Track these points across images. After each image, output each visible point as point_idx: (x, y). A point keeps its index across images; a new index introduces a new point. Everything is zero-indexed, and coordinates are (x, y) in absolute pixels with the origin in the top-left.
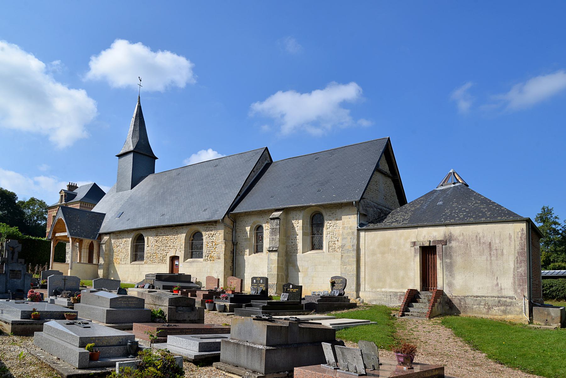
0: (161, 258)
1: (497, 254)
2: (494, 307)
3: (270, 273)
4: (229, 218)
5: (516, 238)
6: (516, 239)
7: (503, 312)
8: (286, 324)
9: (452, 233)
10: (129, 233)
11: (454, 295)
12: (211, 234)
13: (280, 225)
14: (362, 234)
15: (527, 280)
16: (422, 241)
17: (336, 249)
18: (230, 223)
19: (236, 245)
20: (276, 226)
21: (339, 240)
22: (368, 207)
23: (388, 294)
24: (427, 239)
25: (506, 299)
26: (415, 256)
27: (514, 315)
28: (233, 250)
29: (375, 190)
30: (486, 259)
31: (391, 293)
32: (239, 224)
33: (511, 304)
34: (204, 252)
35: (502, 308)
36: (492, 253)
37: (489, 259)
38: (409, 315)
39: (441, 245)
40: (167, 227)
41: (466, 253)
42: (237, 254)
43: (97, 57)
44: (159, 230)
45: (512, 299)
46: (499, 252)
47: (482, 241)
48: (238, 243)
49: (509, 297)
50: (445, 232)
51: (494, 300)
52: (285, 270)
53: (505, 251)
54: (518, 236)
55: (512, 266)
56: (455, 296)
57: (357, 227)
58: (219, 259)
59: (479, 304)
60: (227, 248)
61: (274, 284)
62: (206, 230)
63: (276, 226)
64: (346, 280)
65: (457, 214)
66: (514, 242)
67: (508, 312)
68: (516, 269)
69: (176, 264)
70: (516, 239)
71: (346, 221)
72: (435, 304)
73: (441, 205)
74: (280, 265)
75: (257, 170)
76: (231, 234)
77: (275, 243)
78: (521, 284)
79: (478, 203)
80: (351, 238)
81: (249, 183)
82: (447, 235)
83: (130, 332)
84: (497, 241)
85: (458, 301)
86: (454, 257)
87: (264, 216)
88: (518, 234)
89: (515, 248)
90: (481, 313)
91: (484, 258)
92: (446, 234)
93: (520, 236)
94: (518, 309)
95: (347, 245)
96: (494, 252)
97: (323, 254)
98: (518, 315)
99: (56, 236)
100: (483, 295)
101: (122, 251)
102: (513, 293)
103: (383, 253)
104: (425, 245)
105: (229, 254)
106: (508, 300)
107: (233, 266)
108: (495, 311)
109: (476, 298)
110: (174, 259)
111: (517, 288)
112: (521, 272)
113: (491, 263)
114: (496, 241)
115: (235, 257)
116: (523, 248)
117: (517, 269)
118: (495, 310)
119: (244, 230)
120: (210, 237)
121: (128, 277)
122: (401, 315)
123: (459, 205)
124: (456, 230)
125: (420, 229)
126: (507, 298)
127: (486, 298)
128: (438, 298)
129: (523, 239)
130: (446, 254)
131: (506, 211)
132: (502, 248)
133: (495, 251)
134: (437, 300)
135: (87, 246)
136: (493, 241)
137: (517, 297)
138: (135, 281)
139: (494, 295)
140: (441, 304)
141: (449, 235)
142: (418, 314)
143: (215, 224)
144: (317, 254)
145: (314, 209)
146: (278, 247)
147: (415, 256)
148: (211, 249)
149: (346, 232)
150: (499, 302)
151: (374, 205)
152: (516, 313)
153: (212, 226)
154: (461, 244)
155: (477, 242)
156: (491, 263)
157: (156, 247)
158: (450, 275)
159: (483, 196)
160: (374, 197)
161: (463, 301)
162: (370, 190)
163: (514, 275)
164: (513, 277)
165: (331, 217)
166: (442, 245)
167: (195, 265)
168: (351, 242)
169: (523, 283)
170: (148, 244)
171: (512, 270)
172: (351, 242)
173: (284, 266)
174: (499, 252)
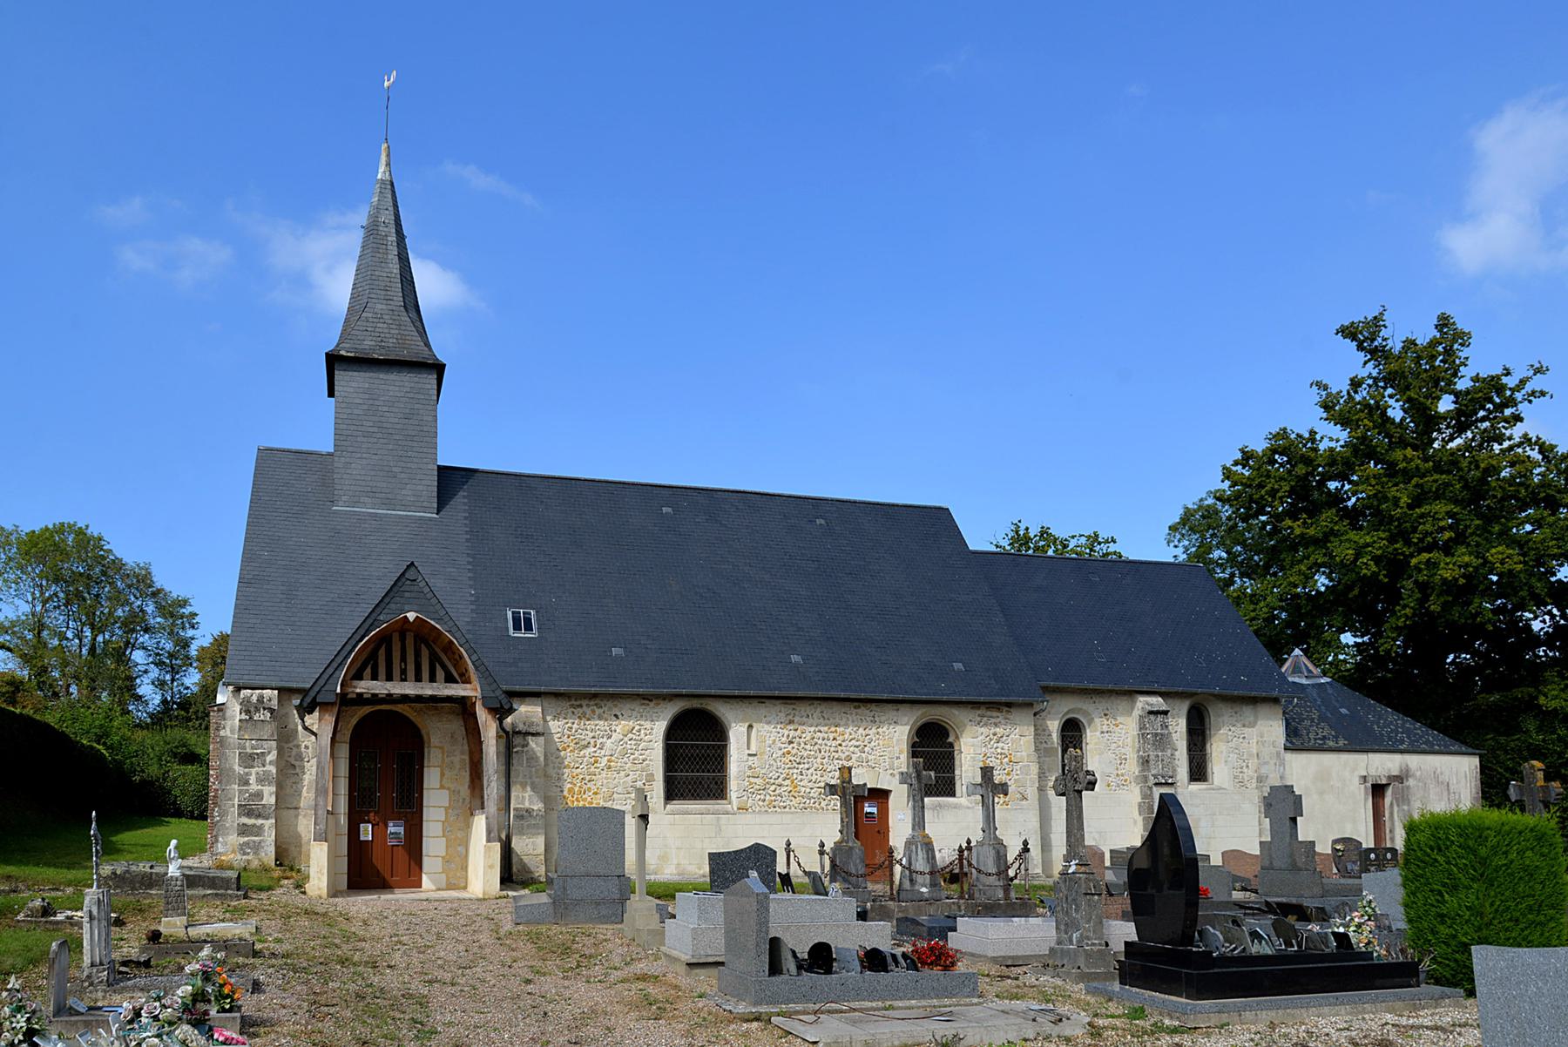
12: (995, 734)
21: (1250, 765)
44: (804, 709)
47: (1440, 780)
69: (867, 813)
80: (1276, 764)
87: (1097, 701)
89: (1471, 792)
103: (1321, 793)
119: (1041, 728)
124: (1414, 761)
143: (1007, 709)
147: (1366, 800)
153: (999, 714)
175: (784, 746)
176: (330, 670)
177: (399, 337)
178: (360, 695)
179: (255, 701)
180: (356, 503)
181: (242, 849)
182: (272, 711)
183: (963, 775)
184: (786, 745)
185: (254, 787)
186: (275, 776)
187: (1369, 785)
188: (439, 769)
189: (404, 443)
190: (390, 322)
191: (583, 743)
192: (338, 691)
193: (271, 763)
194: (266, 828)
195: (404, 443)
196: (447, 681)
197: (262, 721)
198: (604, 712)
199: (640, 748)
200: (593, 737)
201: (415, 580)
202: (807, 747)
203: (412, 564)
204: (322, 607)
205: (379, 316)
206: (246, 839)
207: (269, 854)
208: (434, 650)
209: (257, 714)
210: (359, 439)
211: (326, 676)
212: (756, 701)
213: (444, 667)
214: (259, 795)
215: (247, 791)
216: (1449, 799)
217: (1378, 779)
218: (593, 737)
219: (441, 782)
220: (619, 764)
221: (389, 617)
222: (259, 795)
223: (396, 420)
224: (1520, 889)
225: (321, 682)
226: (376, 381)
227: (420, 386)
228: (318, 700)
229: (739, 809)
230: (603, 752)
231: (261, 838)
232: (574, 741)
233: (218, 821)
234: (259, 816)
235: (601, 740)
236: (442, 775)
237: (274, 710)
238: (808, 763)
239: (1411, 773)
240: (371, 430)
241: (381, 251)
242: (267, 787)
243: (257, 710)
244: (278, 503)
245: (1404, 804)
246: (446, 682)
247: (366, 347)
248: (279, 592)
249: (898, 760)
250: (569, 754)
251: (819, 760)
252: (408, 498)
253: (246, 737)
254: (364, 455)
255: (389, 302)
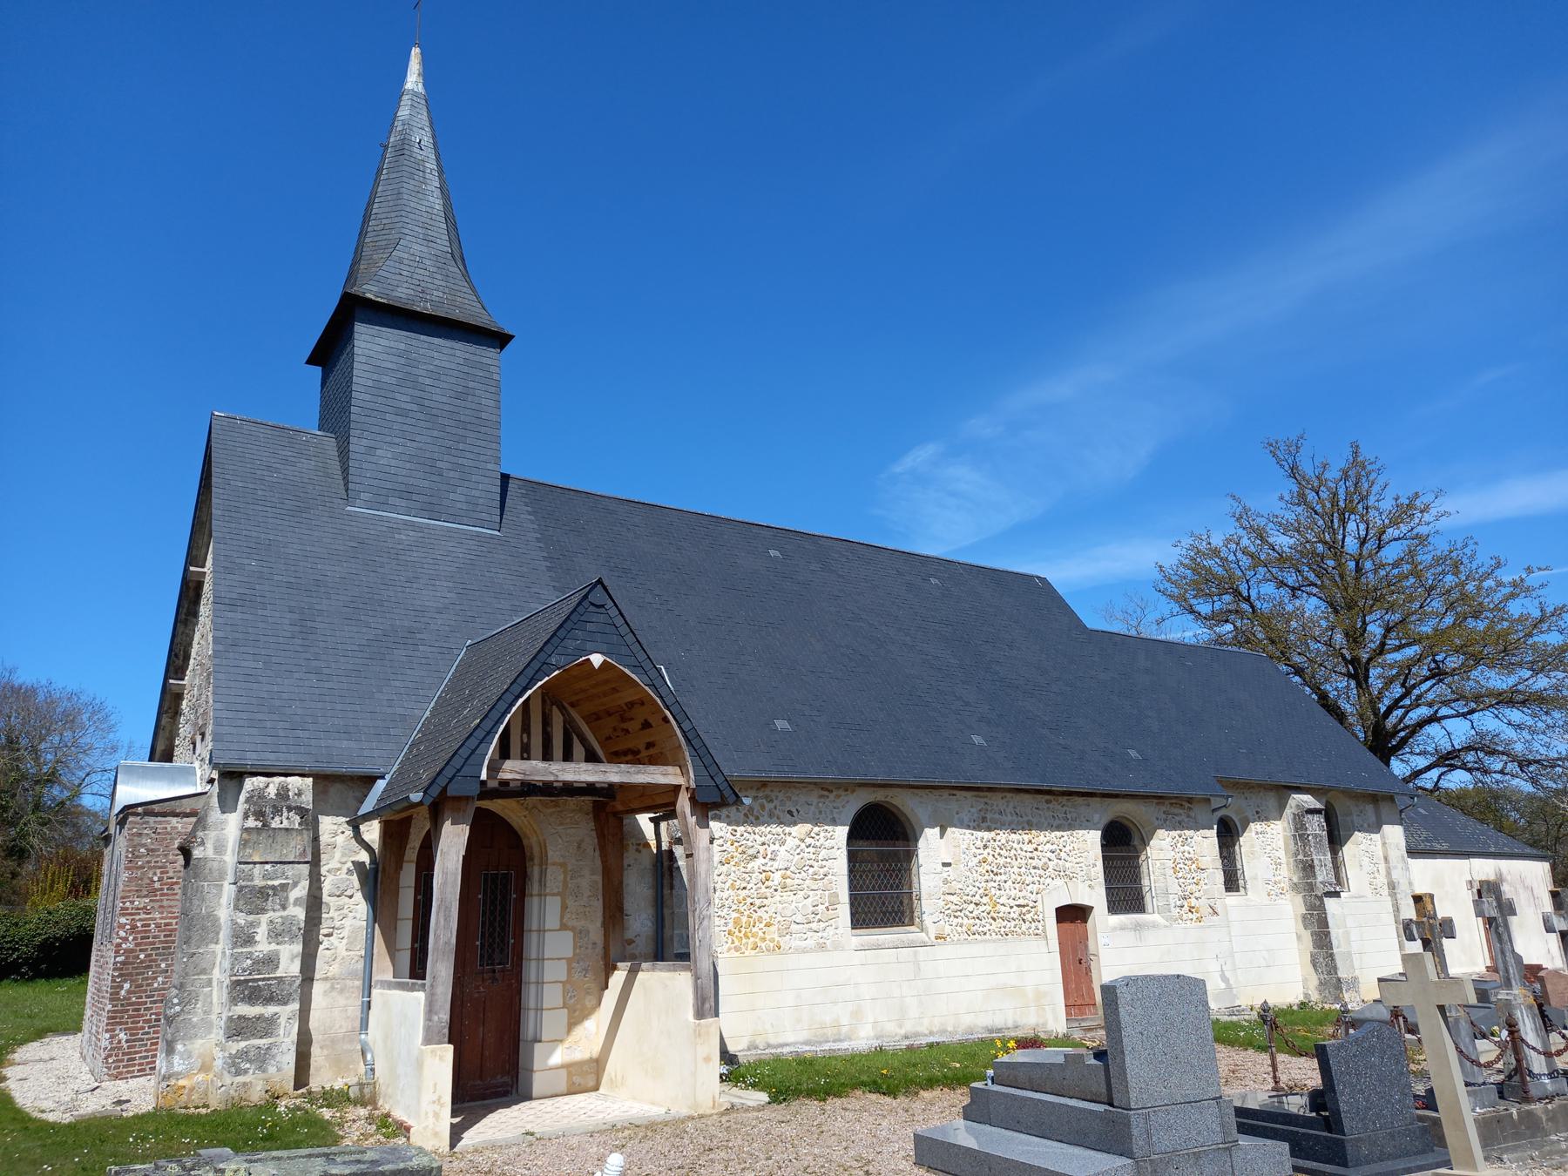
8: (1061, 1060)
10: (832, 796)
43: (70, 720)
44: (997, 801)
83: (484, 1105)
101: (788, 881)
121: (857, 1014)
138: (903, 1032)
153: (1181, 811)
175: (978, 851)
176: (473, 742)
177: (447, 290)
178: (505, 783)
179: (272, 796)
180: (383, 505)
181: (234, 1064)
182: (302, 812)
183: (1153, 885)
184: (981, 851)
185: (263, 946)
186: (302, 925)
188: (559, 898)
189: (454, 431)
190: (435, 269)
191: (751, 852)
192: (484, 776)
193: (297, 902)
194: (282, 1021)
195: (454, 431)
196: (588, 760)
197: (287, 829)
198: (775, 808)
199: (820, 857)
200: (763, 844)
201: (603, 606)
202: (1002, 852)
203: (600, 582)
204: (362, 648)
205: (418, 259)
206: (243, 1044)
207: (285, 1067)
208: (569, 714)
209: (277, 819)
210: (388, 417)
211: (464, 752)
212: (945, 793)
213: (583, 740)
214: (271, 961)
215: (249, 956)
218: (763, 844)
219: (562, 917)
220: (797, 881)
221: (563, 660)
222: (271, 961)
223: (444, 399)
225: (458, 762)
226: (414, 342)
227: (477, 358)
228: (448, 794)
229: (937, 938)
230: (776, 865)
231: (270, 1040)
232: (740, 850)
233: (178, 1014)
234: (270, 1000)
235: (773, 847)
236: (564, 907)
237: (307, 810)
238: (1005, 873)
240: (409, 406)
241: (416, 177)
242: (287, 946)
243: (277, 811)
244: (260, 492)
246: (586, 761)
247: (403, 296)
248: (287, 622)
249: (1095, 869)
250: (733, 868)
251: (1016, 870)
252: (459, 505)
253: (257, 859)
254: (397, 440)
255: (431, 244)
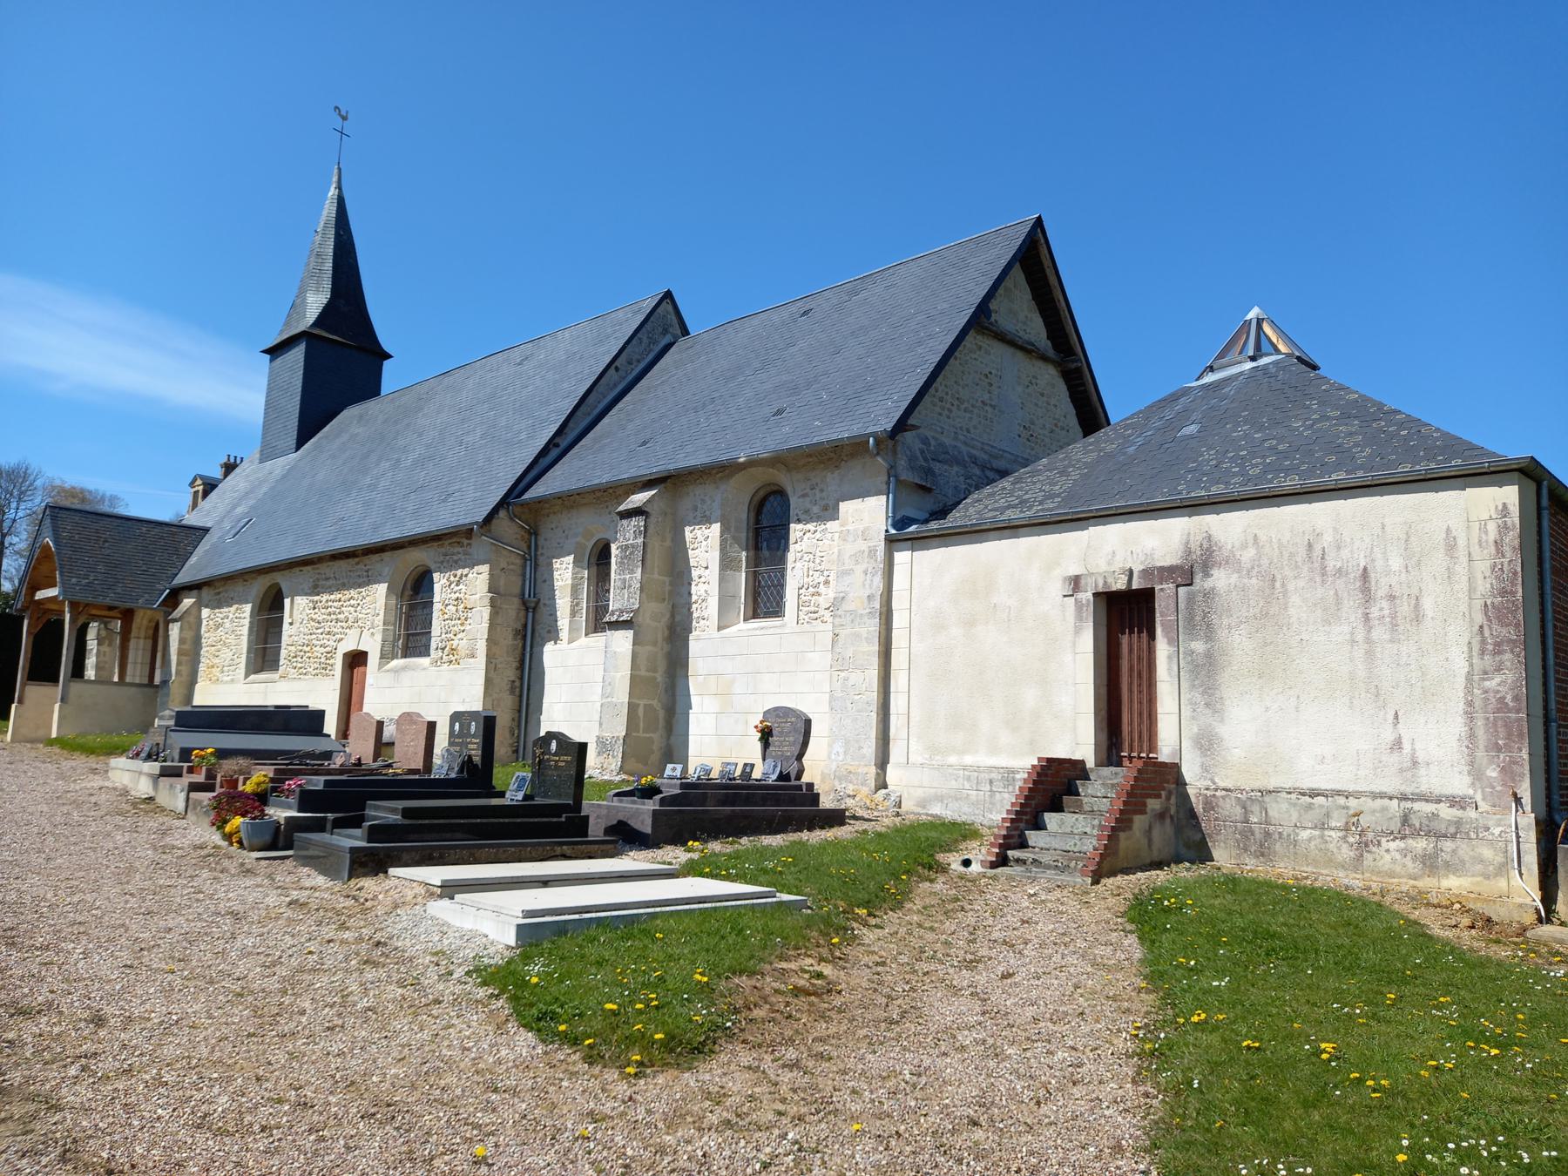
0: (323, 660)
1: (1394, 616)
2: (1383, 840)
3: (609, 700)
4: (511, 519)
5: (1477, 547)
6: (1475, 549)
7: (1424, 864)
9: (1214, 539)
11: (1222, 784)
13: (648, 534)
14: (902, 557)
15: (1525, 724)
16: (1101, 571)
17: (822, 612)
18: (519, 537)
19: (534, 609)
20: (635, 538)
22: (939, 462)
23: (982, 775)
24: (1121, 566)
25: (1436, 806)
26: (1078, 631)
27: (1473, 876)
28: (525, 626)
29: (979, 404)
30: (1348, 637)
31: (991, 772)
32: (546, 540)
33: (1457, 831)
34: (433, 634)
35: (1420, 844)
36: (1375, 612)
37: (1360, 637)
38: (1024, 862)
39: (1171, 585)
40: (341, 559)
41: (1267, 613)
42: (538, 639)
45: (1463, 808)
46: (1405, 608)
47: (1332, 563)
48: (542, 601)
49: (1447, 797)
50: (1189, 534)
51: (1384, 809)
52: (666, 691)
53: (1427, 604)
54: (1483, 536)
55: (1460, 665)
56: (1227, 790)
57: (887, 531)
58: (473, 656)
59: (1322, 826)
60: (499, 620)
61: (618, 737)
62: (442, 562)
63: (635, 538)
64: (808, 722)
65: (1242, 466)
66: (1465, 564)
67: (1447, 864)
68: (1476, 678)
70: (1475, 549)
71: (850, 511)
72: (1131, 821)
73: (1191, 437)
74: (643, 673)
75: (630, 363)
76: (519, 571)
77: (628, 598)
78: (1500, 742)
79: (1329, 418)
80: (866, 573)
81: (596, 406)
82: (1194, 546)
84: (1396, 563)
85: (1239, 810)
86: (1222, 634)
88: (1483, 529)
90: (1330, 862)
91: (1341, 631)
92: (1192, 538)
93: (1493, 533)
94: (1487, 853)
95: (851, 595)
96: (1381, 609)
97: (778, 631)
98: (1487, 877)
99: (37, 598)
100: (1338, 787)
102: (1467, 780)
103: (970, 623)
104: (1114, 589)
105: (507, 639)
106: (1445, 811)
107: (521, 678)
108: (1388, 857)
109: (1308, 799)
110: (356, 660)
111: (1485, 761)
112: (1498, 692)
113: (1370, 654)
114: (1390, 563)
115: (531, 649)
116: (1509, 589)
117: (1484, 679)
118: (1388, 851)
120: (452, 586)
122: (991, 862)
123: (1256, 432)
124: (1229, 527)
125: (1100, 528)
126: (1439, 801)
127: (1352, 802)
128: (1150, 796)
129: (1506, 549)
130: (1190, 618)
131: (1437, 439)
132: (1415, 591)
133: (1385, 604)
134: (1145, 805)
135: (147, 628)
136: (1379, 563)
137: (1484, 799)
139: (1385, 790)
140: (1168, 821)
141: (1201, 545)
142: (1057, 861)
144: (762, 632)
145: (763, 476)
146: (636, 612)
147: (1078, 631)
148: (454, 626)
149: (850, 548)
150: (1405, 820)
151: (971, 456)
152: (1479, 867)
154: (1250, 578)
155: (1311, 570)
156: (1370, 654)
157: (313, 624)
158: (1207, 705)
159: (1356, 392)
160: (975, 427)
161: (1256, 808)
162: (956, 403)
163: (1470, 704)
164: (1466, 713)
165: (808, 499)
166: (1177, 586)
167: (406, 677)
168: (864, 585)
169: (1509, 736)
170: (291, 616)
171: (1461, 681)
172: (862, 586)
173: (660, 677)
174: (1405, 608)
187: (1087, 596)
216: (1366, 617)
217: (1110, 580)
224: (1317, 1118)
239: (1218, 557)
245: (1192, 635)
